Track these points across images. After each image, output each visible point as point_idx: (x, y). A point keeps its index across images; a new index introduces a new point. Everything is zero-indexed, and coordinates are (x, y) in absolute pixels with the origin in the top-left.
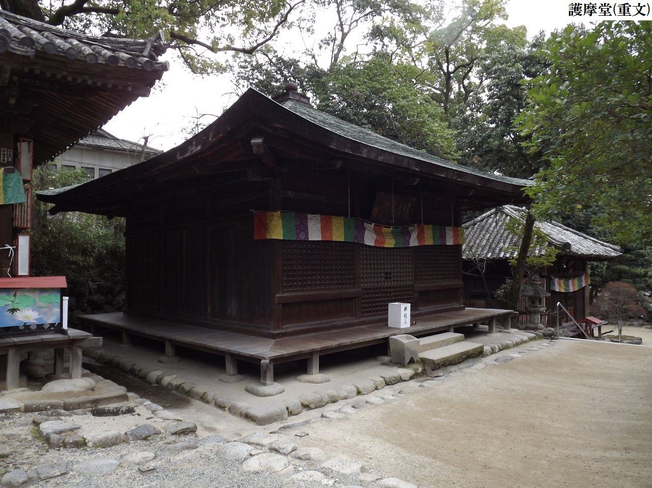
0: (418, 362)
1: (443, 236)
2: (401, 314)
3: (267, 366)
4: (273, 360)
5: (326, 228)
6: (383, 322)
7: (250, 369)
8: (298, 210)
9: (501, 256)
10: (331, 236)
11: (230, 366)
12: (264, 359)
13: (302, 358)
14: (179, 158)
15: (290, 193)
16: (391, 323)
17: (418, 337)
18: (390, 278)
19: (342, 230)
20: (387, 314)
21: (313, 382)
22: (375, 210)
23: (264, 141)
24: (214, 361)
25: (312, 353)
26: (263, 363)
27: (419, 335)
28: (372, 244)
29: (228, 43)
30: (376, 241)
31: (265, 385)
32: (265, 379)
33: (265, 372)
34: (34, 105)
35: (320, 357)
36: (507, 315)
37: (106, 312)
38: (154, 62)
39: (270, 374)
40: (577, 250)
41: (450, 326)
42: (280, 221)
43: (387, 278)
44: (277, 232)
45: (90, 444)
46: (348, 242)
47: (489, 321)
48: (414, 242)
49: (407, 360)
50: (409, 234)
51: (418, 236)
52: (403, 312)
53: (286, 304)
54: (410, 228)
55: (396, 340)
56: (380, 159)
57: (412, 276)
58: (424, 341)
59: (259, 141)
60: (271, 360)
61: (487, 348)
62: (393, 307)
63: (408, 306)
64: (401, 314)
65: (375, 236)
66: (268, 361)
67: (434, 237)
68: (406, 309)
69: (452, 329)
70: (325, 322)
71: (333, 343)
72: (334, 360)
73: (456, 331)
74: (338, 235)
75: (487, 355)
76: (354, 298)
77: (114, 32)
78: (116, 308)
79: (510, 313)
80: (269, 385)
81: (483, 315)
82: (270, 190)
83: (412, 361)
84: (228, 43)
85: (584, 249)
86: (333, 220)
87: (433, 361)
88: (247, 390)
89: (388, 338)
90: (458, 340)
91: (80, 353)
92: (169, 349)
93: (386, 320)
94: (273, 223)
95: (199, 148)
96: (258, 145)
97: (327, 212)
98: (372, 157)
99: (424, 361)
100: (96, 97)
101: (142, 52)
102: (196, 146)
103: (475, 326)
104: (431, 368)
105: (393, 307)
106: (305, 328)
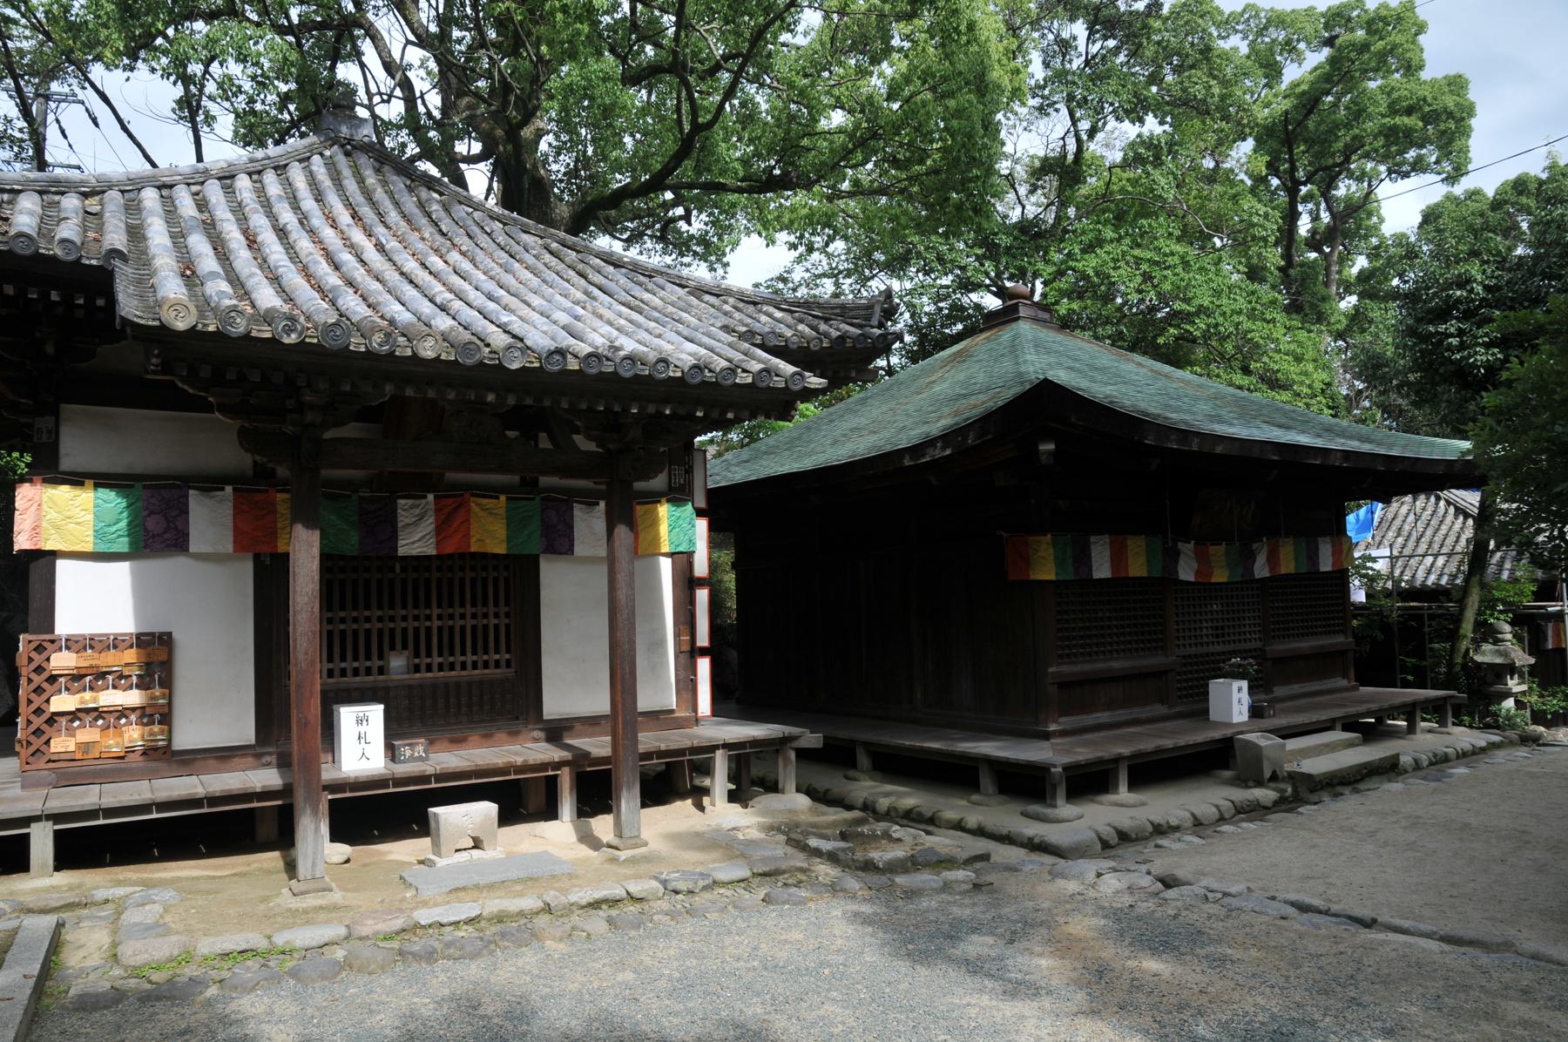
0: (1283, 780)
1: (1313, 557)
2: (1233, 701)
4: (1066, 768)
6: (1200, 712)
7: (1026, 785)
8: (1075, 533)
9: (1429, 583)
11: (986, 781)
14: (907, 462)
16: (1213, 716)
17: (1284, 737)
19: (1142, 559)
20: (1207, 700)
21: (1122, 805)
23: (434, 35)
24: (958, 775)
25: (1117, 760)
27: (1287, 733)
28: (1192, 579)
30: (1198, 573)
32: (1054, 797)
35: (1130, 768)
36: (1445, 699)
41: (1334, 720)
42: (1051, 551)
44: (1046, 571)
47: (1410, 712)
48: (1261, 570)
49: (1267, 774)
50: (1250, 557)
51: (1269, 560)
52: (1235, 696)
53: (1065, 685)
54: (1255, 546)
55: (1247, 742)
56: (1219, 449)
58: (1293, 744)
59: (1052, 446)
61: (1406, 760)
62: (1216, 686)
63: (1244, 684)
64: (1233, 701)
65: (1196, 565)
67: (1296, 559)
68: (1240, 690)
69: (1339, 726)
70: (1122, 714)
71: (1148, 745)
72: (1151, 772)
73: (1346, 728)
74: (1137, 568)
75: (1406, 772)
76: (1166, 672)
79: (1452, 697)
81: (1398, 701)
83: (1274, 777)
86: (1129, 543)
87: (1309, 777)
90: (1350, 744)
91: (793, 755)
92: (863, 760)
93: (1206, 712)
94: (1041, 554)
95: (948, 452)
96: (1048, 452)
97: (1119, 528)
98: (1206, 449)
99: (1293, 777)
103: (1380, 720)
104: (1306, 790)
105: (1216, 686)
106: (1123, 718)
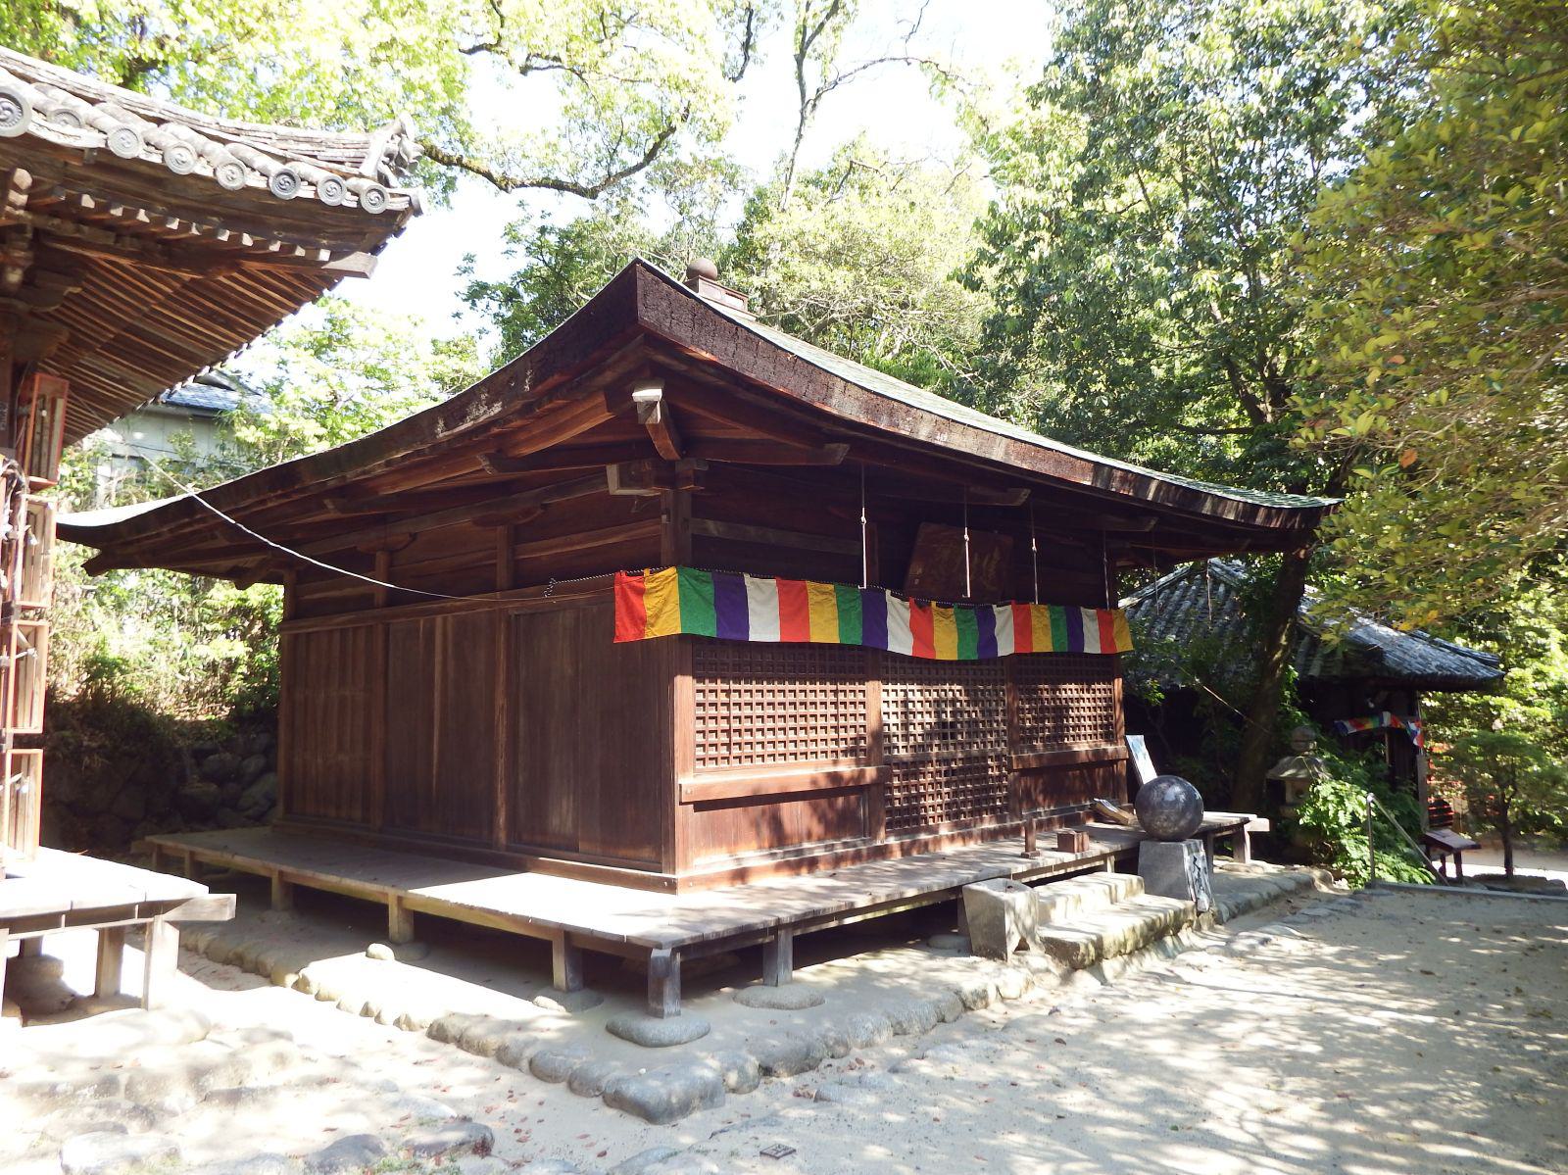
3: (668, 962)
5: (793, 611)
10: (808, 634)
12: (659, 946)
13: (748, 943)
14: (441, 433)
15: (713, 527)
18: (953, 736)
22: (917, 570)
26: (656, 958)
29: (373, 21)
31: (659, 1014)
32: (659, 997)
33: (660, 983)
34: (71, 289)
37: (224, 828)
38: (388, 190)
39: (671, 989)
40: (1399, 664)
43: (945, 736)
45: (696, 1102)
46: (851, 647)
57: (929, 713)
60: (675, 950)
66: (666, 953)
77: (1222, 589)
78: (249, 817)
80: (670, 1015)
82: (664, 517)
84: (373, 21)
85: (1413, 661)
88: (613, 1031)
89: (957, 890)
95: (497, 408)
100: (235, 274)
101: (357, 163)
102: (490, 404)
